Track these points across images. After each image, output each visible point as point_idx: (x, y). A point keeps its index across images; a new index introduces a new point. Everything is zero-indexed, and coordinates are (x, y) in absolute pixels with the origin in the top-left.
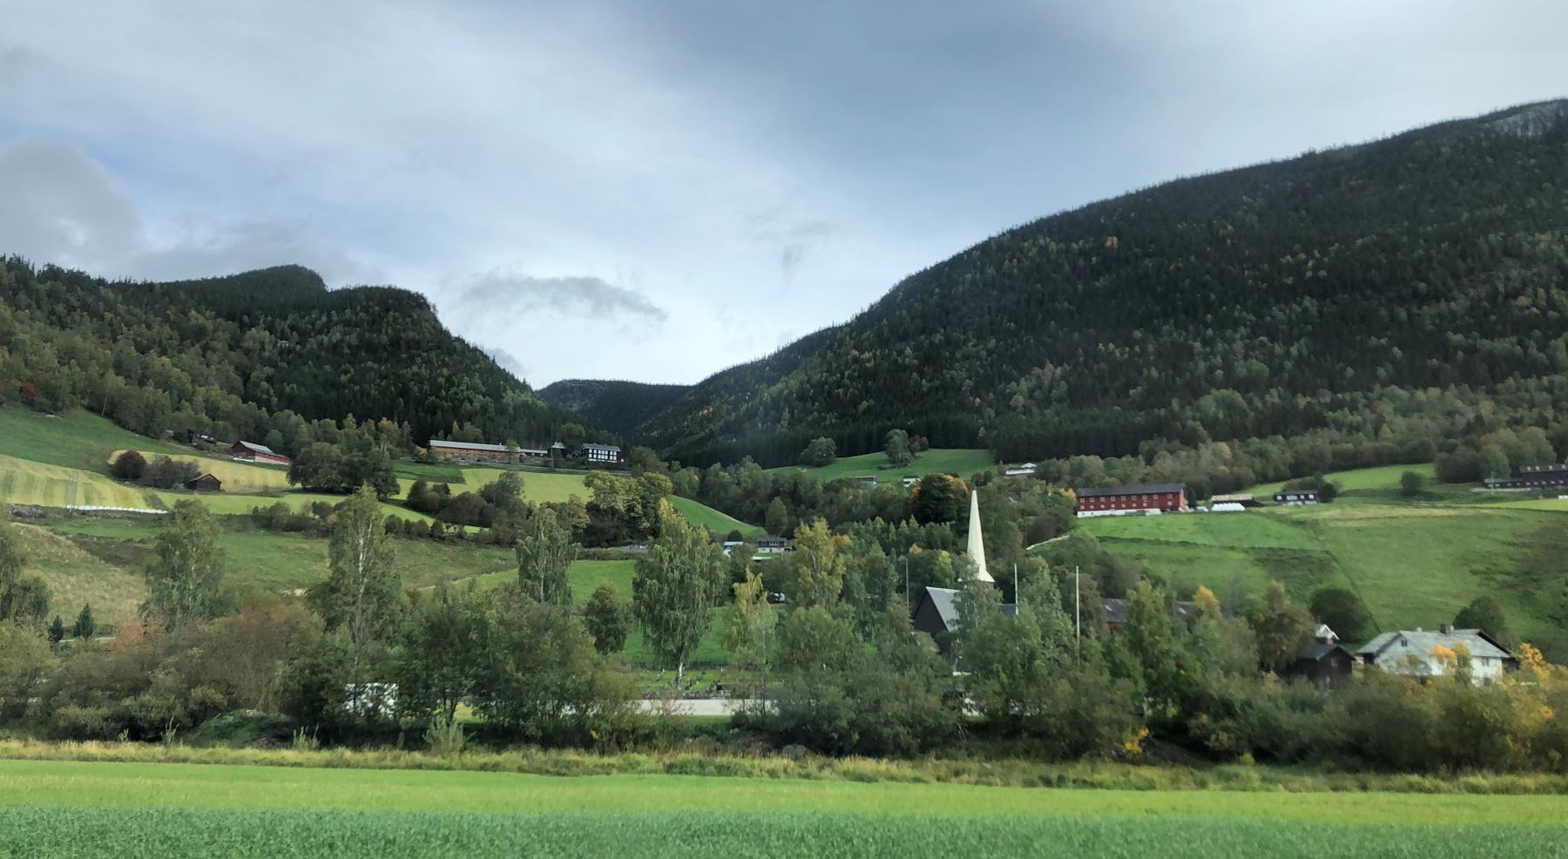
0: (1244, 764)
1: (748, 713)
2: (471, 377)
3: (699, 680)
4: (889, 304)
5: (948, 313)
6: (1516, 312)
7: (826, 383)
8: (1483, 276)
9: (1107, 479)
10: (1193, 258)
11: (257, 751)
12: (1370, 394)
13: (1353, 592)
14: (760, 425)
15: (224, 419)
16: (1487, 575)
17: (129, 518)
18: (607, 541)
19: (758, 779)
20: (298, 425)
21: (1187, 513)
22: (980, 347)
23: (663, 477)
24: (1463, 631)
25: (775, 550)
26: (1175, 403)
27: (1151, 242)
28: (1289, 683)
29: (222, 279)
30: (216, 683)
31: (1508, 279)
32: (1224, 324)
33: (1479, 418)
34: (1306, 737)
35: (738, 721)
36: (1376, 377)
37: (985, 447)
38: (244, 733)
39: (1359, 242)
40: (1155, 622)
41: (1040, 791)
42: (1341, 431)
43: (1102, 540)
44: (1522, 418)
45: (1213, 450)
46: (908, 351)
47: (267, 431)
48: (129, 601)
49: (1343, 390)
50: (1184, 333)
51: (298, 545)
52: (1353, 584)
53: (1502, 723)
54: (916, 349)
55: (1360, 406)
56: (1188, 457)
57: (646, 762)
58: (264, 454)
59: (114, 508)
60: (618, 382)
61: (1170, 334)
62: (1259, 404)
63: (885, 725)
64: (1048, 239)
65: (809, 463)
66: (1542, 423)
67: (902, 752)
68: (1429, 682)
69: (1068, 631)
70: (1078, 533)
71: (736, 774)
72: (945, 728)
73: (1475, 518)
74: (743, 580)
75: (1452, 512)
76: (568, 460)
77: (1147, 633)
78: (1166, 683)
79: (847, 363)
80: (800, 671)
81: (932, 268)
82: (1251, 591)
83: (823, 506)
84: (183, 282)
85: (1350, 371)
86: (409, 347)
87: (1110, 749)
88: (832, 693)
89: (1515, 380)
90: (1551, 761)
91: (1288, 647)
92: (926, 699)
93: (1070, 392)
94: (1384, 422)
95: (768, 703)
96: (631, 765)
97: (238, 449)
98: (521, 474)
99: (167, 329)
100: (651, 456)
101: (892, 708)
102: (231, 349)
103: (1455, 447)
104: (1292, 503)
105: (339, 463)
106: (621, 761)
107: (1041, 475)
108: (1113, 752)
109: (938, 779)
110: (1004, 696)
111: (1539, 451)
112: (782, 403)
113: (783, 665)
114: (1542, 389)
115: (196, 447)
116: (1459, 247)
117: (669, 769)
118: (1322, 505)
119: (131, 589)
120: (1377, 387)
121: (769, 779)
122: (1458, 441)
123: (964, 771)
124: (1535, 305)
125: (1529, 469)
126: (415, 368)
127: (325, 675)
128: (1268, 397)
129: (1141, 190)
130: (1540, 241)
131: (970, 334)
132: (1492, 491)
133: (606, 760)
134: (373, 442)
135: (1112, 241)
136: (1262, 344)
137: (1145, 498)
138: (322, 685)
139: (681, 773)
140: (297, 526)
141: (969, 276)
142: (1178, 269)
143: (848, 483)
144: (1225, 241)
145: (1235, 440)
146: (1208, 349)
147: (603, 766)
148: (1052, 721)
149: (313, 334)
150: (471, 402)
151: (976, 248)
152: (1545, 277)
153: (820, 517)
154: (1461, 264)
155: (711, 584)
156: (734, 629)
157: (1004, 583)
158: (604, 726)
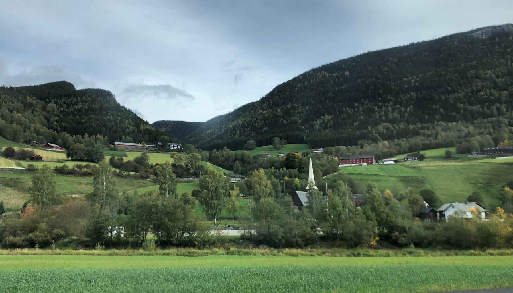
0: (412, 248)
1: (246, 234)
2: (128, 120)
3: (220, 224)
4: (272, 94)
5: (292, 98)
6: (480, 97)
7: (251, 121)
9: (348, 154)
11: (84, 251)
13: (433, 190)
14: (229, 136)
15: (41, 135)
16: (475, 184)
17: (11, 171)
20: (68, 137)
21: (375, 165)
22: (303, 109)
23: (198, 154)
24: (471, 203)
25: (237, 179)
26: (369, 128)
29: (38, 85)
30: (61, 228)
31: (477, 86)
32: (385, 101)
33: (469, 132)
34: (431, 239)
35: (243, 237)
36: (435, 119)
38: (73, 245)
39: (429, 73)
40: (379, 202)
43: (349, 174)
46: (279, 110)
47: (57, 140)
48: (14, 200)
49: (425, 123)
50: (371, 104)
51: (73, 179)
52: (432, 188)
54: (282, 110)
55: (431, 128)
56: (375, 146)
58: (56, 148)
59: (5, 167)
60: (178, 121)
61: (367, 105)
62: (397, 128)
63: (293, 237)
64: (325, 72)
65: (247, 149)
66: (490, 134)
67: (298, 246)
70: (341, 172)
71: (250, 255)
72: (313, 238)
73: (468, 165)
76: (163, 148)
77: (376, 205)
78: (383, 222)
79: (258, 114)
81: (286, 82)
83: (252, 164)
84: (23, 87)
85: (427, 117)
86: (106, 110)
88: (275, 227)
89: (480, 119)
91: (417, 209)
95: (253, 231)
96: (214, 252)
97: (47, 146)
98: (148, 154)
99: (19, 104)
100: (192, 147)
101: (296, 232)
102: (42, 110)
104: (410, 161)
105: (84, 150)
107: (326, 152)
108: (367, 245)
109: (318, 255)
110: (332, 227)
114: (489, 122)
115: (32, 145)
117: (228, 254)
118: (420, 161)
119: (14, 195)
120: (436, 123)
122: (463, 140)
124: (486, 94)
125: (486, 149)
126: (109, 117)
127: (102, 224)
128: (400, 126)
129: (356, 55)
132: (474, 156)
134: (95, 143)
135: (347, 73)
136: (398, 108)
137: (361, 160)
138: (101, 228)
139: (232, 255)
140: (71, 173)
141: (299, 85)
142: (369, 82)
143: (261, 156)
144: (385, 73)
145: (390, 140)
146: (380, 109)
147: (205, 253)
149: (71, 105)
150: (129, 129)
151: (301, 75)
152: (489, 85)
153: (261, 168)
154: (462, 81)
156: (231, 206)
157: (322, 188)
158: (200, 240)
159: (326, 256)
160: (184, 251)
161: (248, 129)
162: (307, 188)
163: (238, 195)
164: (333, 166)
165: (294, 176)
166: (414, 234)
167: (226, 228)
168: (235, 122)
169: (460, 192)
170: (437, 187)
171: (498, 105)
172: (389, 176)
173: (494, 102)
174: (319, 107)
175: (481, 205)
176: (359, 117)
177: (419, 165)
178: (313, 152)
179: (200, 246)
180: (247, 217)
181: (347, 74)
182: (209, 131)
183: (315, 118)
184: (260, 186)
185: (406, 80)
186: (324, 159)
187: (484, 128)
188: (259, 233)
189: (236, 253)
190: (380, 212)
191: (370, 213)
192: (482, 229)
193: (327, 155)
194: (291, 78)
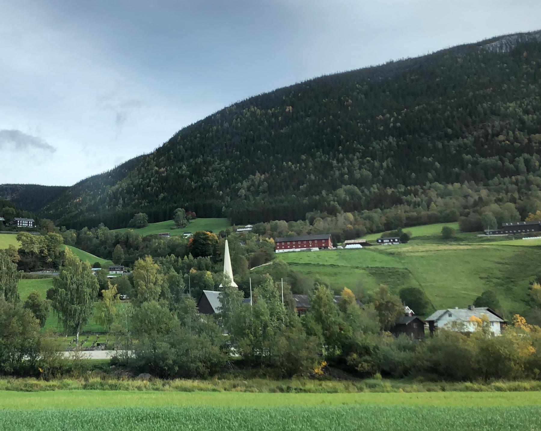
0: (377, 379)
1: (119, 357)
3: (86, 341)
4: (173, 142)
5: (204, 147)
7: (141, 184)
8: (481, 125)
9: (290, 233)
10: (331, 116)
12: (424, 187)
13: (421, 289)
14: (107, 207)
16: (488, 279)
18: (30, 269)
19: (133, 391)
21: (332, 250)
22: (222, 165)
23: (58, 235)
24: (479, 308)
25: (118, 272)
26: (324, 193)
27: (309, 109)
28: (397, 337)
31: (493, 126)
33: (480, 198)
35: (114, 362)
36: (427, 177)
37: (225, 217)
39: (417, 108)
41: (279, 395)
42: (410, 206)
43: (290, 264)
44: (503, 198)
45: (345, 217)
46: (184, 167)
49: (410, 185)
52: (420, 285)
53: (510, 355)
54: (188, 166)
55: (419, 193)
56: (332, 221)
57: (72, 384)
61: (320, 157)
62: (367, 192)
63: (192, 362)
64: (256, 108)
65: (134, 226)
66: (513, 200)
68: (471, 335)
69: (283, 312)
70: (277, 261)
73: (479, 250)
74: (107, 288)
75: (469, 247)
76: (6, 226)
78: (334, 338)
79: (152, 173)
80: (146, 335)
81: (195, 124)
82: (368, 289)
83: (142, 249)
85: (413, 174)
87: (307, 373)
88: (163, 346)
90: (535, 374)
91: (392, 318)
92: (212, 349)
93: (270, 188)
94: (432, 201)
95: (129, 352)
96: (64, 385)
100: (50, 223)
101: (194, 353)
103: (468, 213)
104: (386, 244)
106: (59, 384)
107: (256, 231)
108: (309, 374)
109: (225, 389)
110: (252, 346)
111: (512, 216)
112: (119, 195)
113: (137, 332)
114: (512, 183)
116: (468, 110)
117: (85, 387)
120: (428, 184)
121: (138, 391)
122: (471, 210)
123: (238, 385)
125: (507, 224)
128: (372, 189)
130: (510, 107)
131: (216, 158)
133: (51, 383)
135: (289, 109)
136: (368, 162)
137: (310, 242)
139: (91, 389)
141: (215, 128)
142: (324, 123)
143: (156, 237)
144: (348, 108)
145: (355, 211)
146: (340, 164)
147: (50, 386)
148: (277, 358)
151: (218, 113)
154: (470, 120)
155: (93, 290)
156: (103, 314)
157: (243, 287)
158: (46, 365)
159: (237, 391)
160: (18, 383)
161: (137, 195)
162: (221, 286)
163: (115, 297)
164: (265, 252)
165: (206, 267)
166: (381, 357)
167: (94, 347)
168: (117, 186)
169: (463, 292)
170: (428, 284)
171: (526, 155)
172: (352, 267)
173: (520, 151)
174: (247, 161)
175: (497, 314)
176: (307, 176)
177: (399, 250)
178: (236, 231)
179: (48, 376)
180: (120, 331)
181: (289, 110)
182: (78, 200)
183: (240, 178)
184: (146, 283)
185: (381, 119)
186: (252, 241)
187: (504, 191)
188: (139, 356)
189: (98, 386)
190: (329, 322)
191: (313, 324)
192: (488, 349)
193: (258, 234)
194: (202, 117)
